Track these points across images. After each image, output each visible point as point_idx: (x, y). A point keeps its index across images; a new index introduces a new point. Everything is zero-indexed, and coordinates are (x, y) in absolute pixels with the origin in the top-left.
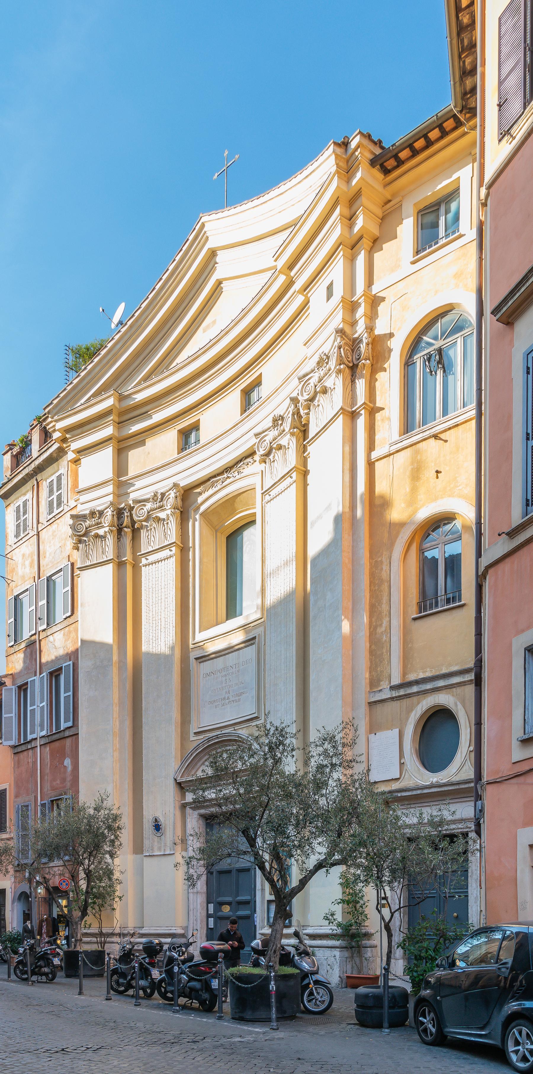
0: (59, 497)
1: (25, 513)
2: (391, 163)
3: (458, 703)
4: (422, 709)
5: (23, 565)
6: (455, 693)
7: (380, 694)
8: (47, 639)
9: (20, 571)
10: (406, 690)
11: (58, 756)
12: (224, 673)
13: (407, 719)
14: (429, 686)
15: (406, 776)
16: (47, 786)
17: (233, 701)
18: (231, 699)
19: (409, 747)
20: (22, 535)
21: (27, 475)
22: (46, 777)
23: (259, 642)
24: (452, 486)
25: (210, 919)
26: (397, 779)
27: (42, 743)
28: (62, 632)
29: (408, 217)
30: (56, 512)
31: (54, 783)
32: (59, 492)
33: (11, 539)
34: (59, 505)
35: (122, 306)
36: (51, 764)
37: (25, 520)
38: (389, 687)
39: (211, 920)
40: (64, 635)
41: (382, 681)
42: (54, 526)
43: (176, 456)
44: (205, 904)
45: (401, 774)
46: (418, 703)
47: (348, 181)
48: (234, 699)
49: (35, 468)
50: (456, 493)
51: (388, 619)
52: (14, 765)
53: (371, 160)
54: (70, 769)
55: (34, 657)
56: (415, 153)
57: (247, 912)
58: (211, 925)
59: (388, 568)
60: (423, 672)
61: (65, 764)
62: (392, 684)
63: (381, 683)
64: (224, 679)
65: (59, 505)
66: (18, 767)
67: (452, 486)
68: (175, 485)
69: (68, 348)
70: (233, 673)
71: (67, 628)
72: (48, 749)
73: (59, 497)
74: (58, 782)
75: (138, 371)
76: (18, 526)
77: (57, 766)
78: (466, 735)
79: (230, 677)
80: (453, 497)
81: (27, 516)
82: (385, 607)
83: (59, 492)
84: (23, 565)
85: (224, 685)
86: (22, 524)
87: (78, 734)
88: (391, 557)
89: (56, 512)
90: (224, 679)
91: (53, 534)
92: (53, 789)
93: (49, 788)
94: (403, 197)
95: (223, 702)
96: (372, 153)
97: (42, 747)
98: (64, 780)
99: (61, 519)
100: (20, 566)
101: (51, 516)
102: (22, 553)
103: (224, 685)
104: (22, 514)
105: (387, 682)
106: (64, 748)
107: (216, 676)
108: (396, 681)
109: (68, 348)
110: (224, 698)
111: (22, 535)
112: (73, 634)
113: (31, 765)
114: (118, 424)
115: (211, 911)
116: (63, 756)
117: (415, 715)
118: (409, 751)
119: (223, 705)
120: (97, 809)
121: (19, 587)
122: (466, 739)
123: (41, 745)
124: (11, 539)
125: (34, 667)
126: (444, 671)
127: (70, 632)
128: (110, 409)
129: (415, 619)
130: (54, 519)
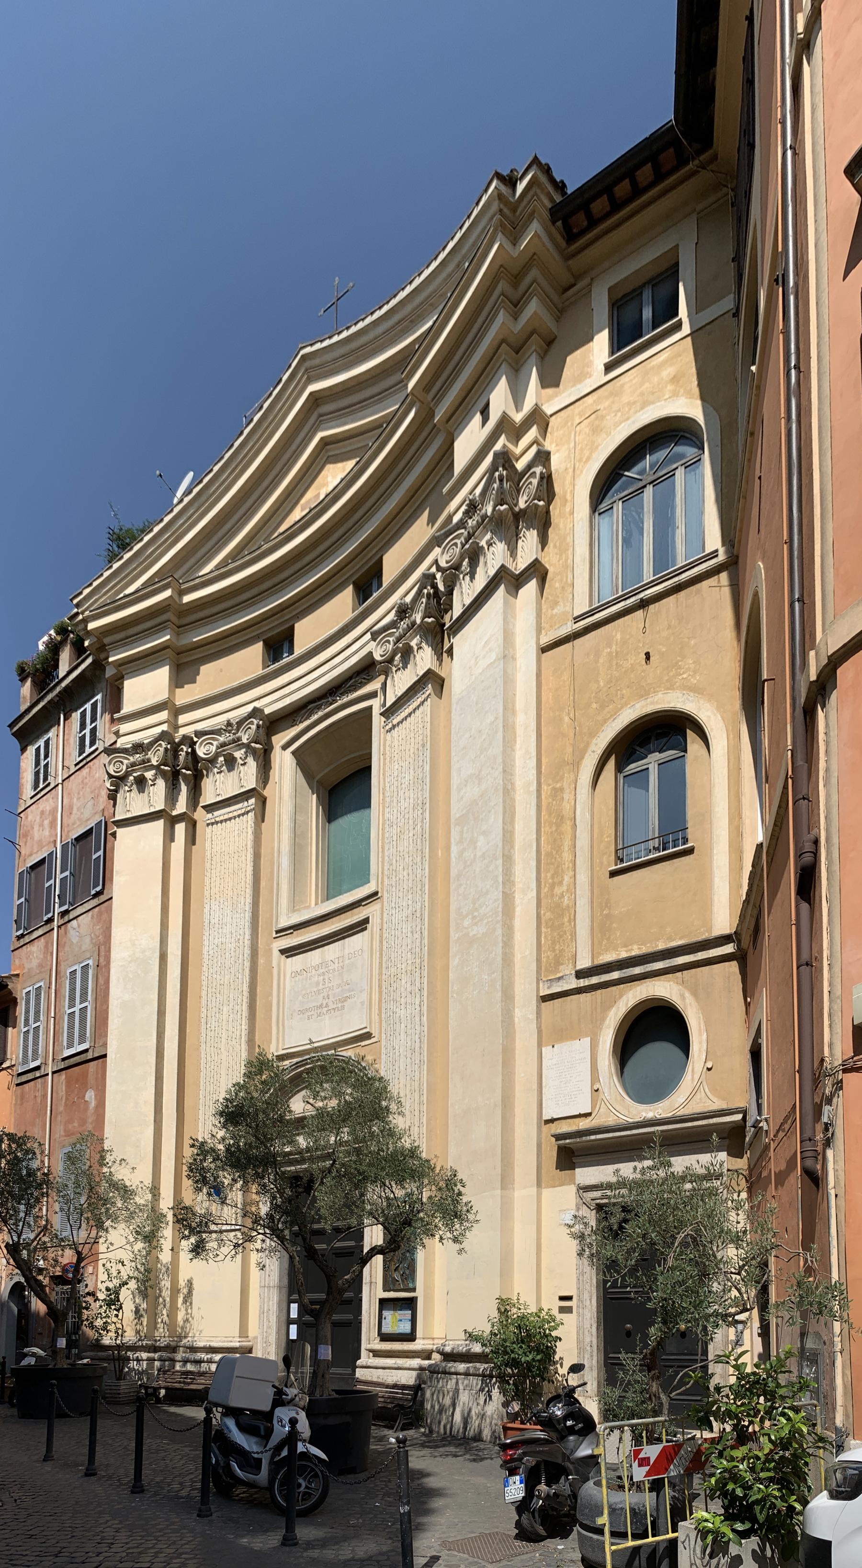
0: (94, 731)
1: (46, 756)
2: (580, 220)
3: (687, 994)
4: (627, 1004)
5: (41, 825)
6: (680, 981)
7: (561, 983)
8: (69, 925)
9: (36, 834)
10: (598, 977)
11: (79, 1086)
12: (321, 971)
13: (603, 1020)
14: (637, 970)
15: (601, 1110)
16: (59, 1130)
17: (334, 1009)
18: (331, 1006)
19: (607, 1063)
20: (41, 786)
21: (49, 702)
22: (59, 1118)
23: (372, 931)
24: (671, 674)
25: (292, 1305)
26: (588, 1115)
27: (55, 1069)
28: (90, 913)
29: (600, 330)
30: (88, 750)
31: (70, 1126)
32: (93, 725)
33: (28, 791)
34: (92, 743)
35: (191, 474)
36: (67, 1099)
37: (46, 766)
38: (573, 972)
39: (293, 1329)
40: (92, 917)
41: (562, 964)
42: (85, 771)
43: (260, 672)
44: (284, 1328)
45: (593, 1106)
46: (621, 996)
47: (515, 242)
48: (335, 1006)
49: (60, 692)
50: (678, 684)
51: (571, 873)
52: (16, 1100)
53: (550, 209)
54: (93, 1104)
55: (50, 950)
56: (616, 206)
57: (350, 1317)
58: (293, 1335)
59: (572, 797)
60: (627, 951)
61: (87, 1098)
62: (579, 967)
63: (561, 967)
64: (322, 978)
65: (92, 743)
66: (22, 1104)
67: (671, 674)
68: (256, 713)
69: (111, 532)
70: (334, 970)
71: (97, 908)
72: (64, 1077)
73: (94, 731)
74: (76, 1124)
75: (206, 624)
76: (37, 774)
77: (75, 1103)
78: (700, 1043)
79: (331, 975)
80: (673, 689)
81: (49, 759)
82: (567, 856)
83: (93, 725)
84: (41, 825)
85: (321, 987)
86: (42, 771)
87: (105, 1056)
88: (576, 781)
89: (88, 750)
90: (322, 978)
91: (82, 782)
92: (68, 1134)
93: (62, 1133)
94: (592, 279)
95: (319, 1011)
96: (552, 200)
97: (55, 1075)
98: (83, 1122)
99: (95, 761)
100: (36, 828)
101: (81, 757)
102: (41, 809)
103: (321, 987)
104: (42, 756)
105: (570, 966)
106: (85, 1075)
107: (309, 975)
108: (584, 963)
109: (111, 532)
110: (321, 1006)
111: (41, 786)
112: (105, 916)
113: (39, 1100)
114: (179, 627)
115: (294, 1314)
116: (85, 1087)
117: (616, 1014)
118: (607, 1068)
119: (319, 1016)
120: (121, 529)
121: (34, 856)
122: (700, 1050)
123: (53, 1073)
124: (28, 791)
125: (49, 963)
126: (661, 946)
127: (100, 913)
128: (167, 603)
129: (613, 874)
130: (85, 762)
